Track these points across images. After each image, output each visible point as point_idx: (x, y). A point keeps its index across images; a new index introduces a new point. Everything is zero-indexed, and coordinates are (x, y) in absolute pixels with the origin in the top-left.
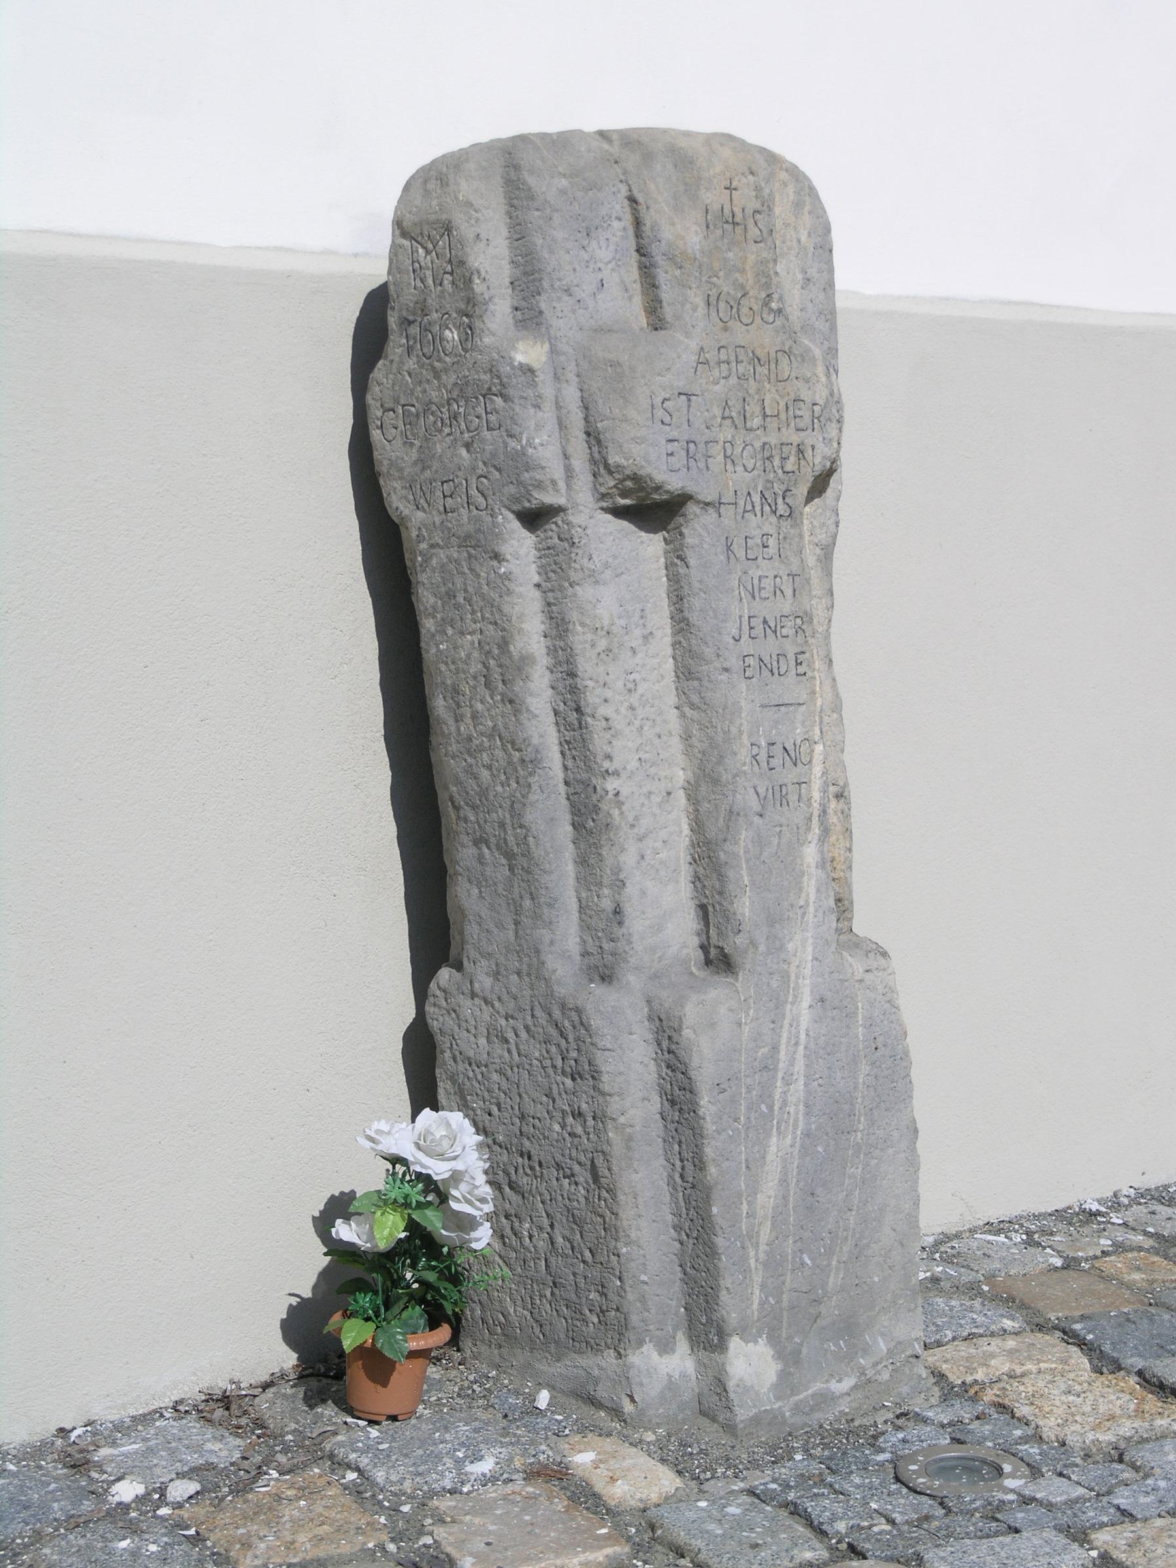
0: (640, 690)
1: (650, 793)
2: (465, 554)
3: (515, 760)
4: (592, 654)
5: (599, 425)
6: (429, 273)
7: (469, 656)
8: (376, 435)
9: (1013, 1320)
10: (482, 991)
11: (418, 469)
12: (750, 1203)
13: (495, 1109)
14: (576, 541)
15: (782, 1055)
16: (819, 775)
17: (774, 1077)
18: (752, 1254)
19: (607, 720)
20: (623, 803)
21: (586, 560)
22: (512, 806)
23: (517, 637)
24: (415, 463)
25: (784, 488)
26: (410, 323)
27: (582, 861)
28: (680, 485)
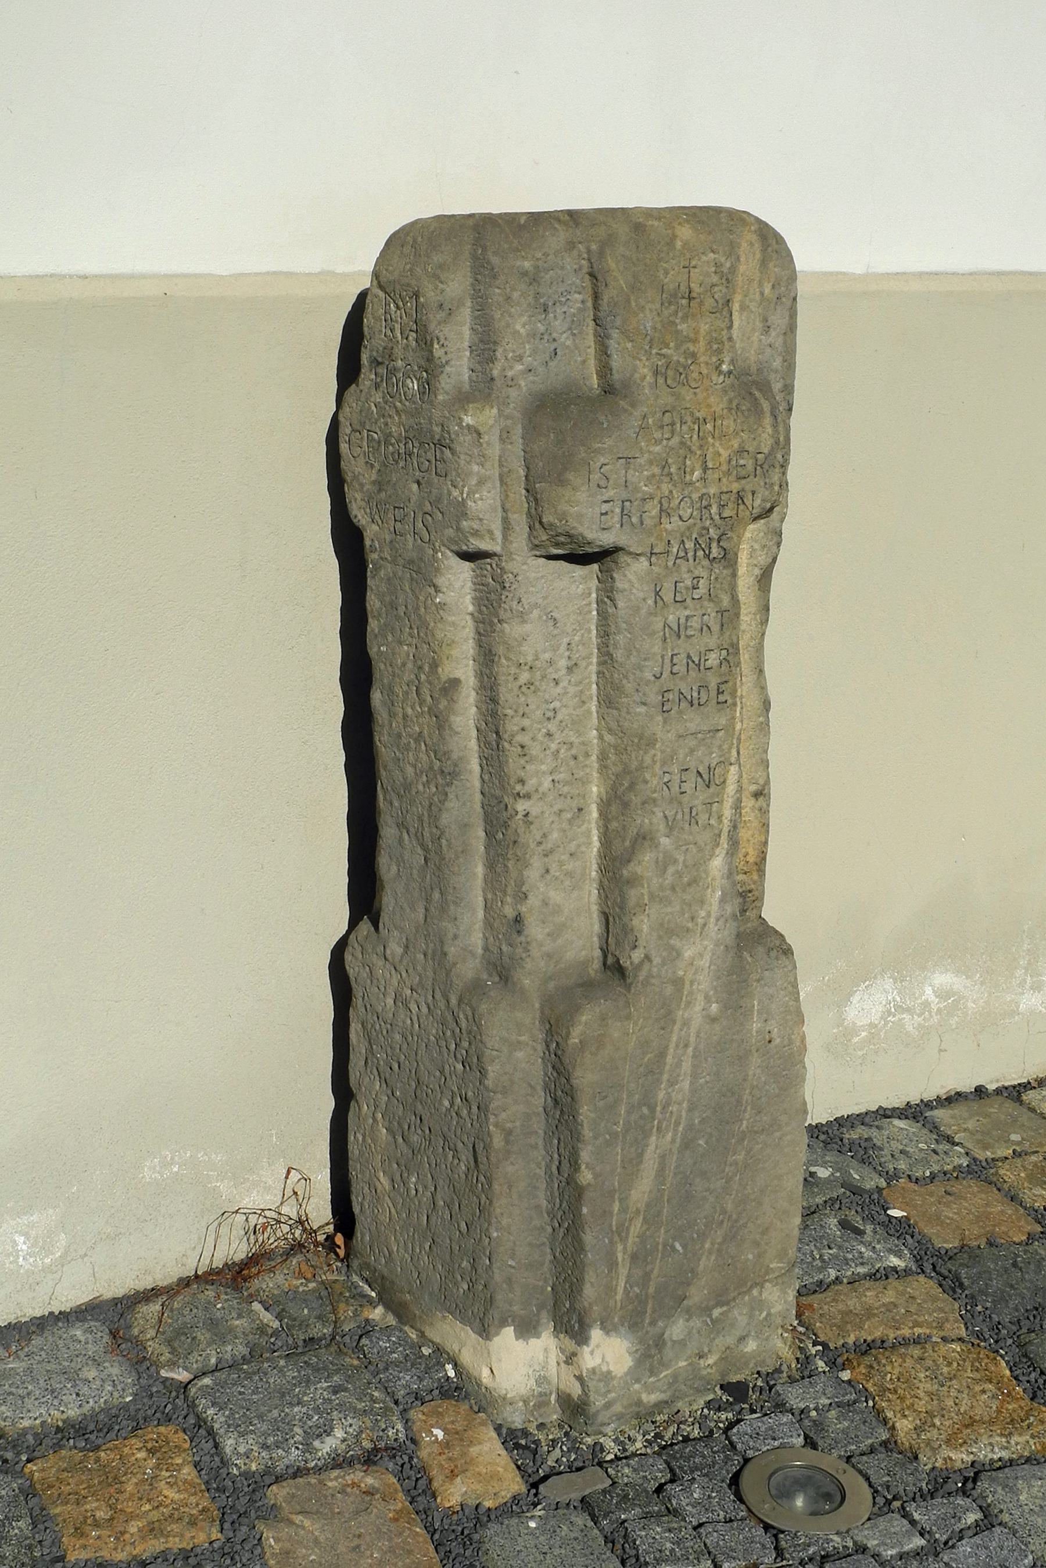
0: (559, 717)
1: (561, 811)
2: (408, 575)
3: (436, 768)
4: (514, 686)
5: (537, 485)
6: (397, 326)
7: (404, 665)
8: (344, 447)
9: (900, 1257)
10: (393, 958)
11: (375, 489)
12: (621, 1200)
13: (395, 1066)
14: (507, 585)
15: (669, 1059)
16: (732, 793)
17: (659, 1081)
18: (620, 1247)
19: (522, 747)
20: (531, 823)
21: (515, 603)
22: (430, 807)
23: (446, 662)
24: (374, 483)
25: (719, 532)
26: (379, 364)
27: (491, 866)
28: (611, 541)
